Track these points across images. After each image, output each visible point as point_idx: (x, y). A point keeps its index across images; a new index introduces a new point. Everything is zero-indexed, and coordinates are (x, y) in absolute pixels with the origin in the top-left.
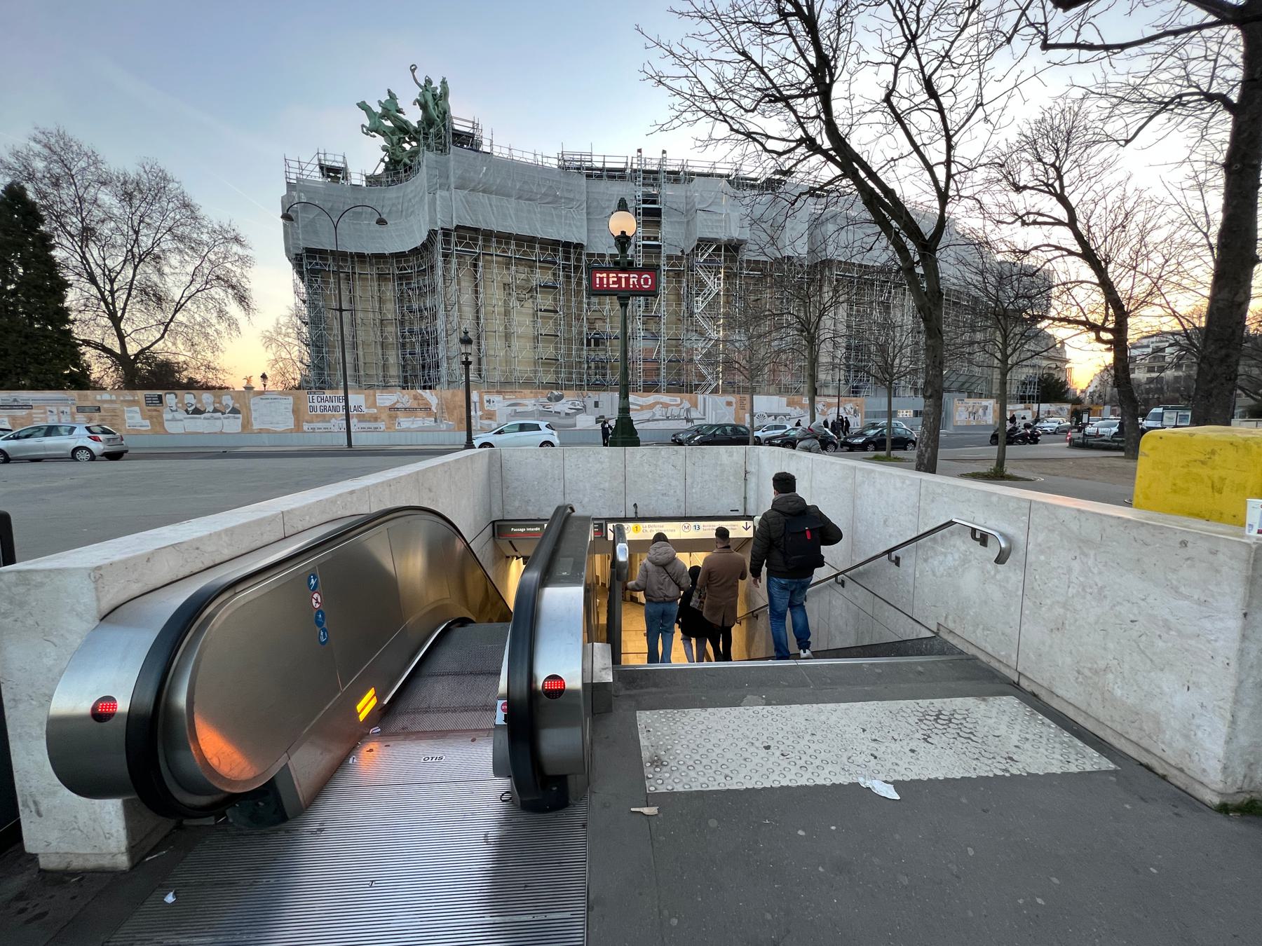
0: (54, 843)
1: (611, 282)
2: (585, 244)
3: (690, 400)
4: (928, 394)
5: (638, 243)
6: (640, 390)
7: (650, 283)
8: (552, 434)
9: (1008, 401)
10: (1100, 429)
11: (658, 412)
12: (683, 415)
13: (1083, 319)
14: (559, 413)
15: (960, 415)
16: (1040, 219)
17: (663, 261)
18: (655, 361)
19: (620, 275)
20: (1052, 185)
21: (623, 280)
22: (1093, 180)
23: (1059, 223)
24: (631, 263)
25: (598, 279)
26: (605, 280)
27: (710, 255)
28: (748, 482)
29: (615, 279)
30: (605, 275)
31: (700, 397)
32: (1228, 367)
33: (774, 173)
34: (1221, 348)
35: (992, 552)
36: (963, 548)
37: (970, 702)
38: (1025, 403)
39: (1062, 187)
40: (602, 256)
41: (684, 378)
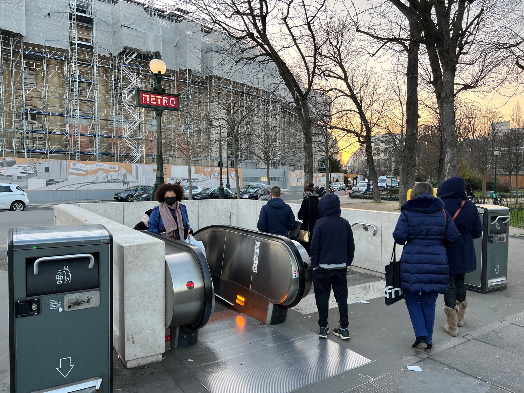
0: (138, 354)
1: (152, 101)
2: (24, 34)
3: (126, 168)
4: (307, 171)
5: (74, 42)
6: (78, 158)
7: (175, 103)
8: (23, 195)
9: (314, 171)
10: (360, 188)
11: (101, 176)
12: (121, 178)
13: (353, 130)
14: (11, 176)
15: (293, 180)
16: (332, 74)
17: (95, 59)
18: (90, 136)
19: (157, 97)
20: (336, 58)
21: (159, 100)
22: (353, 59)
23: (340, 78)
24: (164, 90)
25: (143, 98)
26: (148, 99)
27: (132, 60)
28: (231, 219)
29: (154, 99)
30: (148, 96)
31: (134, 165)
32: (413, 160)
33: (176, 10)
34: (410, 152)
35: (371, 232)
36: (359, 233)
37: (372, 283)
38: (322, 173)
39: (341, 59)
41: (114, 151)
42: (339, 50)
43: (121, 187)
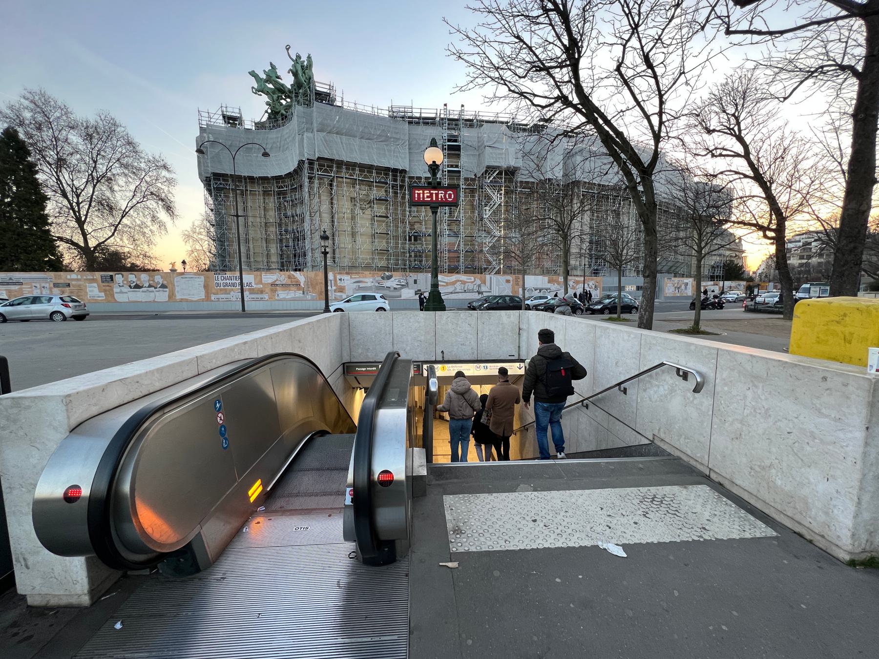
0: (38, 588)
1: (425, 197)
2: (407, 170)
3: (481, 279)
4: (646, 275)
5: (445, 169)
6: (446, 272)
7: (453, 197)
8: (385, 303)
9: (702, 279)
10: (766, 299)
11: (459, 287)
12: (476, 289)
13: (755, 222)
14: (389, 288)
15: (669, 289)
16: (724, 153)
17: (462, 182)
18: (456, 251)
19: (432, 192)
20: (733, 129)
21: (434, 195)
22: (761, 126)
23: (738, 155)
24: (439, 183)
25: (416, 195)
26: (421, 195)
27: (494, 178)
28: (521, 336)
29: (429, 195)
30: (421, 192)
31: (488, 277)
32: (855, 255)
33: (539, 121)
34: (851, 242)
35: (691, 384)
36: (671, 382)
37: (676, 489)
38: (714, 280)
39: (740, 130)
40: (419, 178)
42: (737, 118)
43: (476, 296)
